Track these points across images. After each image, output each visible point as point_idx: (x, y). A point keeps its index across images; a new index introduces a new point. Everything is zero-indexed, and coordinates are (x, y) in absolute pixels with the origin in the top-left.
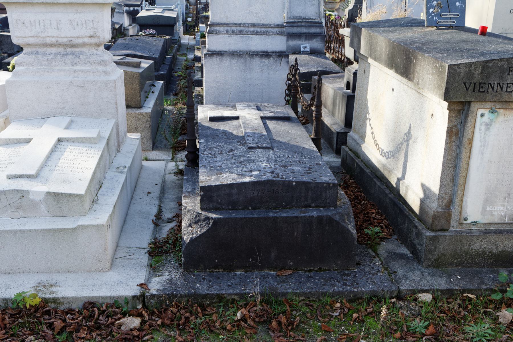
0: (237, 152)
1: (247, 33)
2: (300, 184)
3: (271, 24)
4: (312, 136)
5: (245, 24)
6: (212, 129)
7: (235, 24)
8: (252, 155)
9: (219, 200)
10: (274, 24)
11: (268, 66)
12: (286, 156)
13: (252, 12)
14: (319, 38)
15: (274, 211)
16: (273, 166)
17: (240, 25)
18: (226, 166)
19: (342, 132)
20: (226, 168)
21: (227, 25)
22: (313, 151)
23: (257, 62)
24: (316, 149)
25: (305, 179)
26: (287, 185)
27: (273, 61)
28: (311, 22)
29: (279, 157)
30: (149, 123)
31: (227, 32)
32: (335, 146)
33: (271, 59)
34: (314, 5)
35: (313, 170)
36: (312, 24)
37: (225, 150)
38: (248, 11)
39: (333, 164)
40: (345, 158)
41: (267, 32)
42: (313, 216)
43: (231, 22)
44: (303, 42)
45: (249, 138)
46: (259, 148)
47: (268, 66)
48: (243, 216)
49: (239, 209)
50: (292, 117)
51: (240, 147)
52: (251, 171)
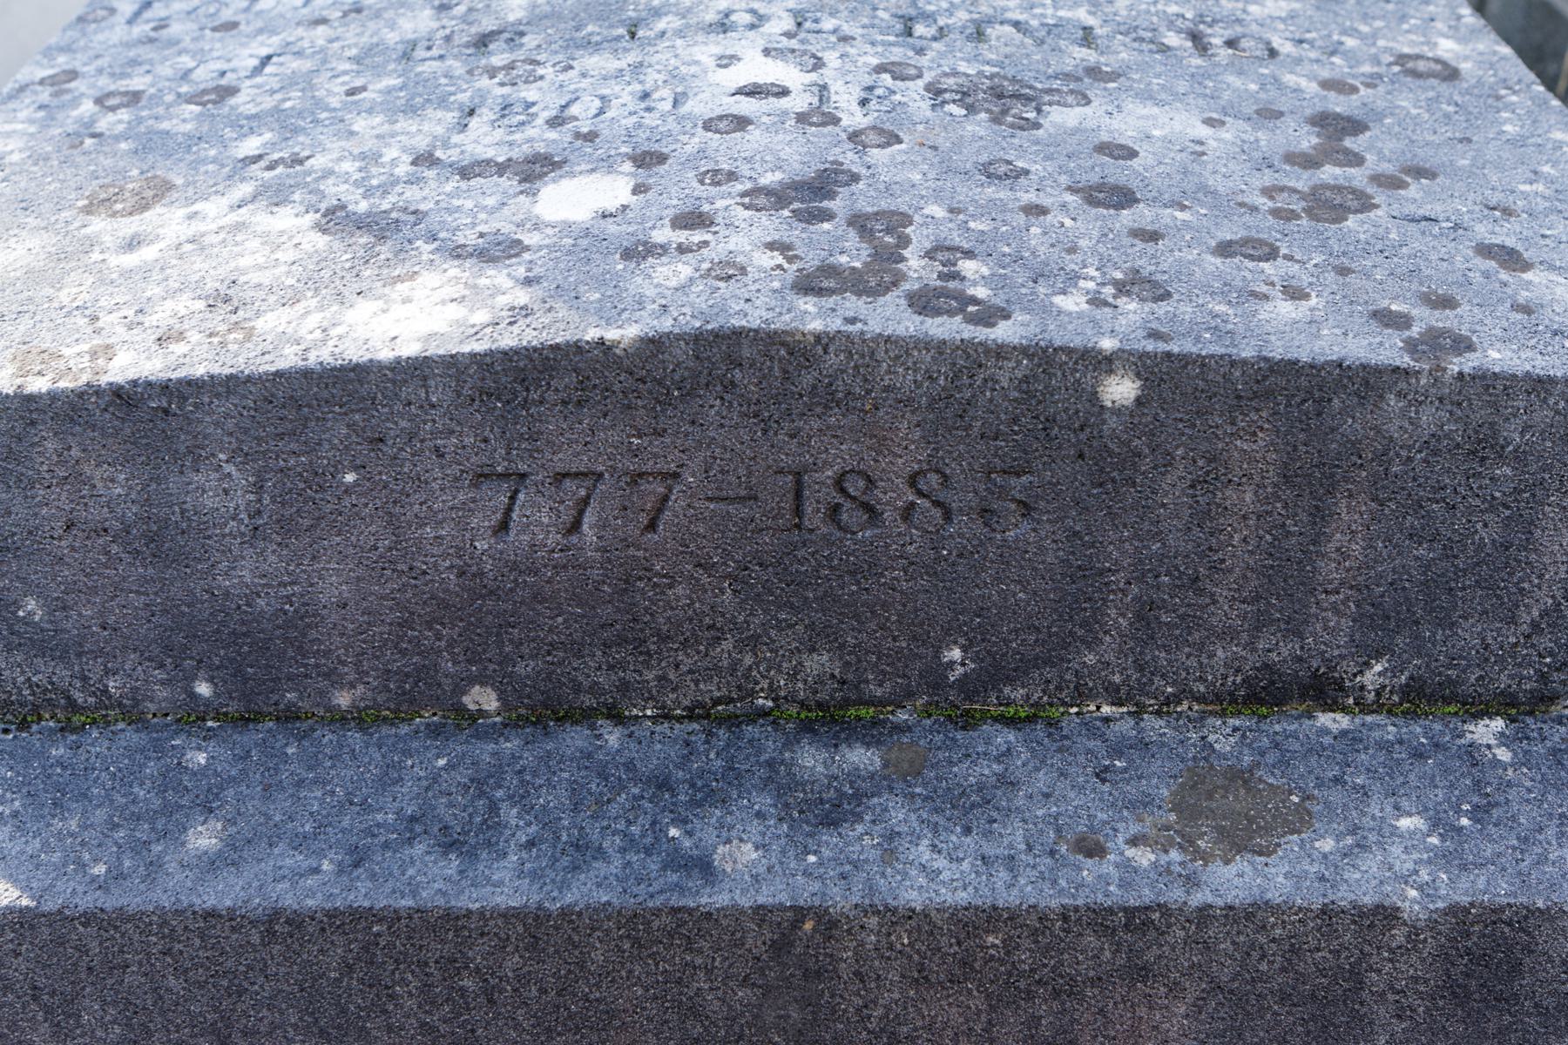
15: (810, 759)
16: (845, 99)
18: (290, 82)
20: (253, 123)
25: (1300, 321)
26: (1017, 421)
35: (1377, 150)
42: (1386, 914)
48: (306, 882)
49: (340, 719)
52: (536, 169)
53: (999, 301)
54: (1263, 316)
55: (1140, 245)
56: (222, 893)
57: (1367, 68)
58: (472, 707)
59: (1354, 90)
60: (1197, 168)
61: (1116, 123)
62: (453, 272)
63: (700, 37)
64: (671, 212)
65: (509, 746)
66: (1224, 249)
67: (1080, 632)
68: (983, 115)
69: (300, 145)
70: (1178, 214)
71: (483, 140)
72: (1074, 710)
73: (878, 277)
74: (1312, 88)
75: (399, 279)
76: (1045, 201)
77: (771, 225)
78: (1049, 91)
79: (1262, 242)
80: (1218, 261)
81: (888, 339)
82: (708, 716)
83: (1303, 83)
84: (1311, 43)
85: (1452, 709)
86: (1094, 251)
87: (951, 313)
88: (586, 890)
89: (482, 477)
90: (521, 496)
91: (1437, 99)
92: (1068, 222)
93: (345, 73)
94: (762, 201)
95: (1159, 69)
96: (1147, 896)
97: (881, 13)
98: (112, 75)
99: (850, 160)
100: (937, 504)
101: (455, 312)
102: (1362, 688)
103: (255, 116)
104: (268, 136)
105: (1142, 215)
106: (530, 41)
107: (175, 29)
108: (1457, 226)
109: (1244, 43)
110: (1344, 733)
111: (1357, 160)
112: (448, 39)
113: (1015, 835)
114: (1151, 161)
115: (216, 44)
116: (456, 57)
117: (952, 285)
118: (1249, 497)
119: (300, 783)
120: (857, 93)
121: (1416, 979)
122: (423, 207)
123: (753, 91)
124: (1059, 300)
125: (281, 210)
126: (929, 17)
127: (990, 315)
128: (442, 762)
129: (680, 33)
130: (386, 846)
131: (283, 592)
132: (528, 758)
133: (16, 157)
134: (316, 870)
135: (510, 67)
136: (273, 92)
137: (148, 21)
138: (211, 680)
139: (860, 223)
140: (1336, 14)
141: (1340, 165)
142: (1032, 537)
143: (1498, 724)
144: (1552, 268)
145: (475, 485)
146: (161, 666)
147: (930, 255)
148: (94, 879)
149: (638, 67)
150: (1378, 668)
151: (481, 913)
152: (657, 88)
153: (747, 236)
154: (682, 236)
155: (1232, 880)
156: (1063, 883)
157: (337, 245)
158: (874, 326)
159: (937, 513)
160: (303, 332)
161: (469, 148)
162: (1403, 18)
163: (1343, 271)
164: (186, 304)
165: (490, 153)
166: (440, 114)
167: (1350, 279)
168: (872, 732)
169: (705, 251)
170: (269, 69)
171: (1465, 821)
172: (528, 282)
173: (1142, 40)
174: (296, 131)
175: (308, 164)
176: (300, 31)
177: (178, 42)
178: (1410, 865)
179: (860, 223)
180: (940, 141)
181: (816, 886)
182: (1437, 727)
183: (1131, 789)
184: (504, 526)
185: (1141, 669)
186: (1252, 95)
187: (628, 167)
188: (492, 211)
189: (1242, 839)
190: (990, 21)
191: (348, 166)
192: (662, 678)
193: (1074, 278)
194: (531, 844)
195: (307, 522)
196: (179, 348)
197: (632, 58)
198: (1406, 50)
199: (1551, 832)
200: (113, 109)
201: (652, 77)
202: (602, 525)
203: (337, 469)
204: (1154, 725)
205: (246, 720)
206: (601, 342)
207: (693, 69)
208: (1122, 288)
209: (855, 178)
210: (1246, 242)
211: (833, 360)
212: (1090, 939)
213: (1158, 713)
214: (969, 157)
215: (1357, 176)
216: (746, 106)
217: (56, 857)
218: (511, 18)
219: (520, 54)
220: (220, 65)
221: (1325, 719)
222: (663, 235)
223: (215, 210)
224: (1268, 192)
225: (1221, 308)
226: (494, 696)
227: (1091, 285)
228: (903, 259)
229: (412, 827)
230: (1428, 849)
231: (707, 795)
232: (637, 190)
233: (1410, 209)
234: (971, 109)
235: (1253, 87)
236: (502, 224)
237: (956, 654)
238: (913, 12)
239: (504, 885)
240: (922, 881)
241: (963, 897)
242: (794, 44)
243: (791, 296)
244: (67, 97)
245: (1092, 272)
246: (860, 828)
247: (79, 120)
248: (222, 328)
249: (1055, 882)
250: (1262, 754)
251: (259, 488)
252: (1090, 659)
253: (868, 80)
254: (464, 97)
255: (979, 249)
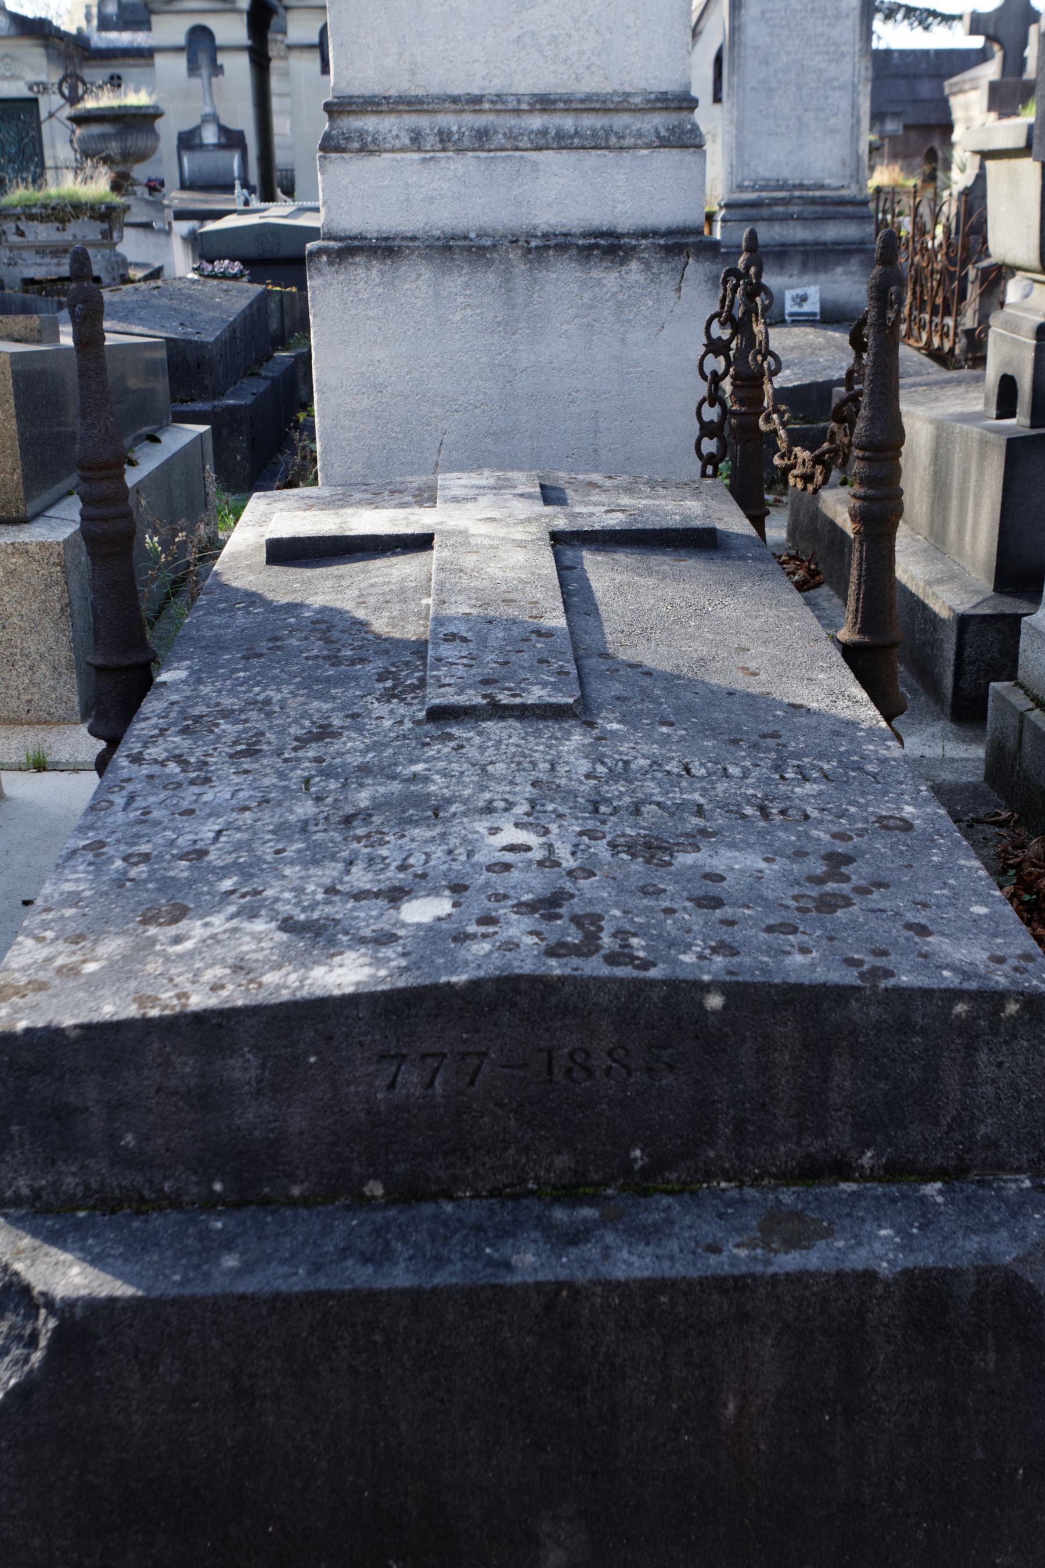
0: (351, 747)
1: (514, 143)
2: (760, 1003)
3: (627, 95)
4: (845, 634)
5: (499, 98)
6: (267, 604)
7: (455, 100)
8: (437, 768)
9: (129, 1139)
10: (645, 92)
11: (620, 305)
12: (673, 767)
13: (533, 35)
14: (855, 261)
15: (560, 1214)
16: (563, 851)
17: (475, 101)
18: (238, 847)
19: (984, 618)
20: (224, 871)
21: (412, 104)
22: (852, 724)
23: (564, 281)
24: (869, 714)
25: (805, 963)
26: (660, 1016)
27: (641, 278)
28: (823, 201)
29: (624, 772)
30: (57, 590)
31: (416, 140)
32: (948, 681)
33: (634, 265)
34: (834, 131)
35: (858, 873)
36: (830, 209)
37: (282, 731)
38: (515, 33)
39: (947, 776)
40: (1011, 744)
41: (608, 132)
42: (869, 1276)
43: (435, 90)
44: (794, 280)
45: (448, 651)
46: (497, 711)
47: (620, 305)
48: (294, 1280)
49: (293, 1203)
50: (728, 535)
51: (379, 709)
52: (396, 895)
53: (651, 958)
54: (787, 962)
55: (725, 928)
56: (247, 1286)
57: (860, 825)
58: (368, 1194)
59: (851, 838)
60: (758, 886)
61: (715, 862)
62: (363, 950)
63: (477, 817)
64: (474, 917)
65: (391, 1213)
66: (770, 929)
67: (705, 1138)
68: (640, 859)
69: (256, 883)
70: (746, 911)
71: (360, 878)
72: (705, 1185)
73: (589, 946)
74: (826, 837)
75: (333, 955)
76: (676, 906)
77: (528, 922)
78: (678, 844)
79: (790, 925)
80: (765, 935)
81: (595, 978)
82: (500, 1195)
83: (822, 835)
84: (829, 810)
85: (913, 1178)
86: (700, 931)
87: (626, 964)
88: (442, 1278)
89: (383, 1057)
90: (403, 1068)
91: (897, 843)
92: (687, 917)
93: (270, 840)
94: (523, 909)
95: (740, 829)
96: (744, 1269)
97: (580, 800)
98: (127, 843)
99: (568, 886)
100: (624, 1066)
101: (368, 971)
102: (862, 1167)
103: (222, 868)
104: (235, 879)
105: (728, 912)
106: (377, 819)
107: (156, 814)
108: (896, 914)
109: (791, 812)
110: (854, 1192)
111: (847, 879)
112: (326, 819)
113: (674, 1245)
114: (733, 882)
115: (186, 824)
116: (335, 830)
117: (626, 950)
118: (787, 1057)
119: (277, 1235)
120: (569, 848)
121: (893, 1317)
122: (337, 917)
123: (512, 848)
124: (682, 957)
125: (257, 921)
126: (607, 801)
127: (646, 965)
128: (355, 1222)
129: (465, 814)
130: (332, 1262)
131: (270, 1126)
132: (402, 1219)
133: (87, 893)
134: (296, 1274)
135: (368, 836)
136: (230, 853)
137: (137, 809)
138: (223, 1181)
139: (576, 920)
140: (846, 792)
141: (837, 882)
142: (675, 1083)
143: (938, 1185)
144: (943, 934)
145: (379, 1062)
146: (196, 1173)
147: (614, 935)
148: (175, 1282)
149: (443, 835)
150: (869, 1154)
151: (389, 1291)
152: (456, 848)
153: (517, 928)
154: (483, 929)
155: (790, 1261)
156: (699, 1265)
157: (294, 938)
158: (587, 972)
159: (623, 1071)
160: (289, 983)
161: (356, 884)
162: (886, 793)
163: (831, 939)
164: (218, 971)
165: (368, 886)
166: (333, 864)
167: (836, 943)
168: (592, 1201)
169: (496, 937)
170: (223, 839)
171: (915, 1231)
172: (404, 955)
173: (731, 811)
174: (252, 875)
175: (265, 893)
176: (235, 815)
177: (161, 823)
178: (883, 1252)
179: (576, 920)
180: (617, 875)
181: (567, 1272)
182: (905, 1187)
183: (737, 1223)
184: (392, 1085)
185: (739, 1158)
186: (792, 843)
187: (447, 893)
188: (377, 918)
189: (792, 1244)
190: (643, 802)
191: (287, 895)
192: (475, 1173)
193: (689, 946)
194: (411, 1258)
195: (286, 1085)
196: (224, 993)
197: (438, 830)
198: (884, 813)
199: (960, 1234)
200: (136, 864)
201: (453, 841)
202: (446, 1082)
203: (307, 1054)
204: (750, 1192)
205: (241, 1204)
206: (448, 983)
207: (476, 836)
208: (714, 950)
209: (572, 896)
210: (781, 925)
211: (568, 989)
212: (715, 1297)
213: (752, 1186)
214: (633, 883)
215: (845, 888)
216: (509, 857)
217: (151, 1272)
218: (362, 805)
219: (372, 828)
220: (191, 837)
221: (844, 1186)
222: (472, 928)
223: (218, 922)
224: (796, 898)
225: (765, 959)
226: (381, 1186)
227: (698, 949)
228: (600, 938)
229: (344, 1253)
230: (894, 1243)
231: (504, 1233)
232: (455, 905)
233: (872, 905)
234: (634, 856)
235: (793, 838)
236: (383, 925)
237: (638, 1153)
238: (598, 798)
239: (400, 1277)
240: (624, 1267)
241: (646, 1274)
242: (531, 819)
243: (544, 958)
244: (104, 857)
245: (699, 942)
246: (589, 1245)
247: (117, 871)
248: (244, 982)
249: (695, 1265)
250: (808, 1203)
251: (263, 1066)
252: (712, 1154)
253: (575, 840)
254: (345, 854)
255: (641, 932)
